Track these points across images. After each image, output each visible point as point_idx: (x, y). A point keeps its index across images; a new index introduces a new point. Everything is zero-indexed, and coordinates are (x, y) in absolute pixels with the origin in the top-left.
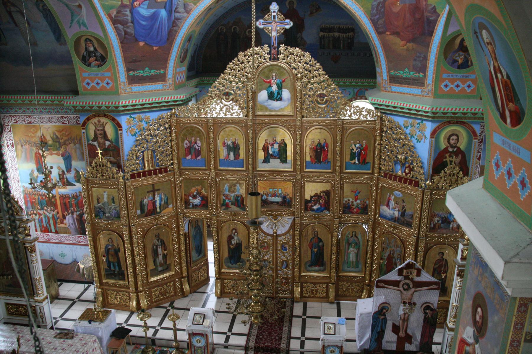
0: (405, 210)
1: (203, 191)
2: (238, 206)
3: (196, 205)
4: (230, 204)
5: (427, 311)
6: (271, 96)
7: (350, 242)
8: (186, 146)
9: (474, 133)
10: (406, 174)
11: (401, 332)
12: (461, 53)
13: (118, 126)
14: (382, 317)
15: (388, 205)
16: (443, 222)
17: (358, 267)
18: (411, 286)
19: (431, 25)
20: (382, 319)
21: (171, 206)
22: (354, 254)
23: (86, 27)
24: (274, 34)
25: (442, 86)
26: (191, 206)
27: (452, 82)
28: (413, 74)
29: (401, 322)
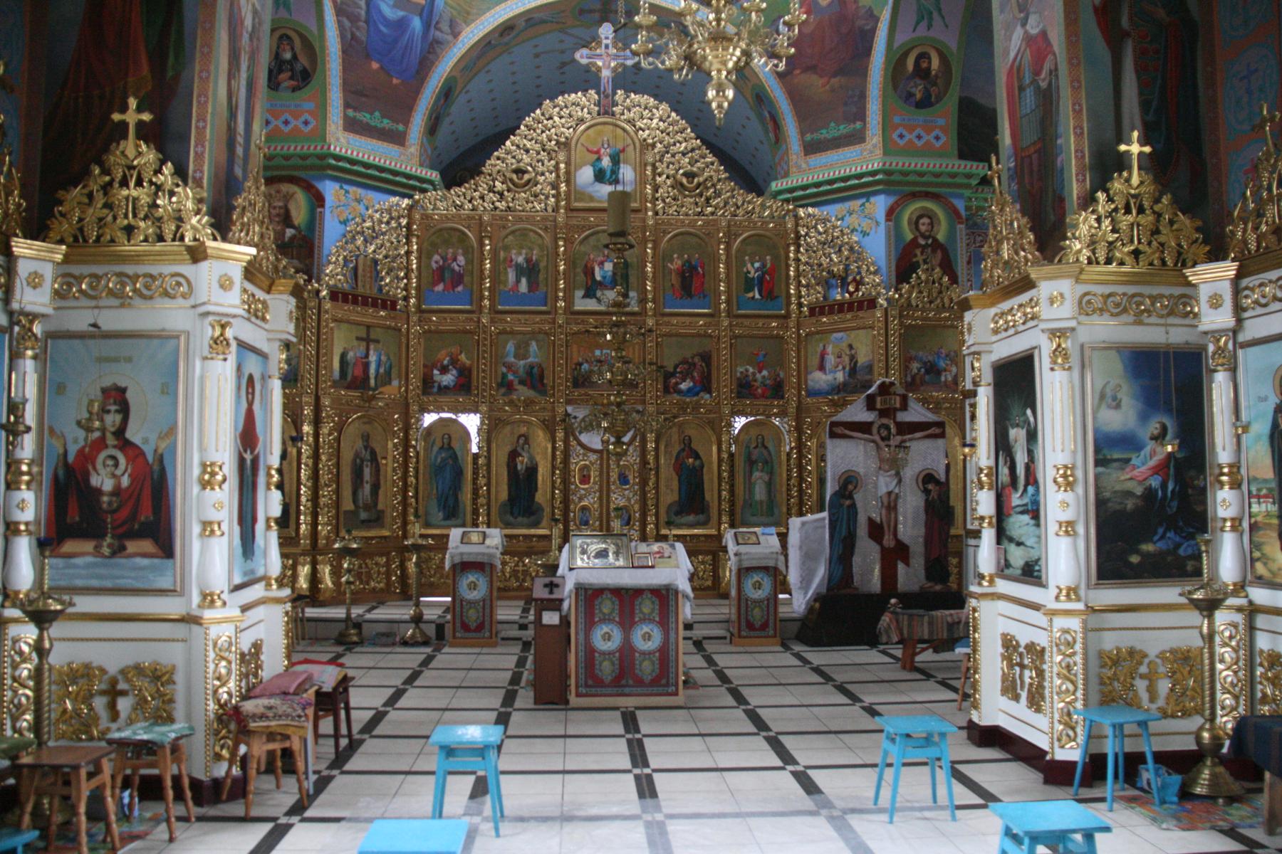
0: (856, 363)
1: (463, 357)
2: (532, 387)
3: (446, 387)
4: (516, 382)
5: (930, 487)
6: (600, 176)
7: (754, 457)
8: (434, 266)
9: (956, 212)
10: (851, 294)
11: (886, 537)
12: (918, 81)
13: (319, 199)
14: (848, 502)
15: (822, 368)
16: (927, 372)
17: (772, 515)
18: (893, 430)
19: (866, 39)
20: (849, 507)
21: (395, 383)
22: (763, 486)
23: (289, 10)
24: (606, 73)
25: (895, 136)
26: (435, 390)
27: (911, 130)
28: (844, 129)
29: (884, 512)
